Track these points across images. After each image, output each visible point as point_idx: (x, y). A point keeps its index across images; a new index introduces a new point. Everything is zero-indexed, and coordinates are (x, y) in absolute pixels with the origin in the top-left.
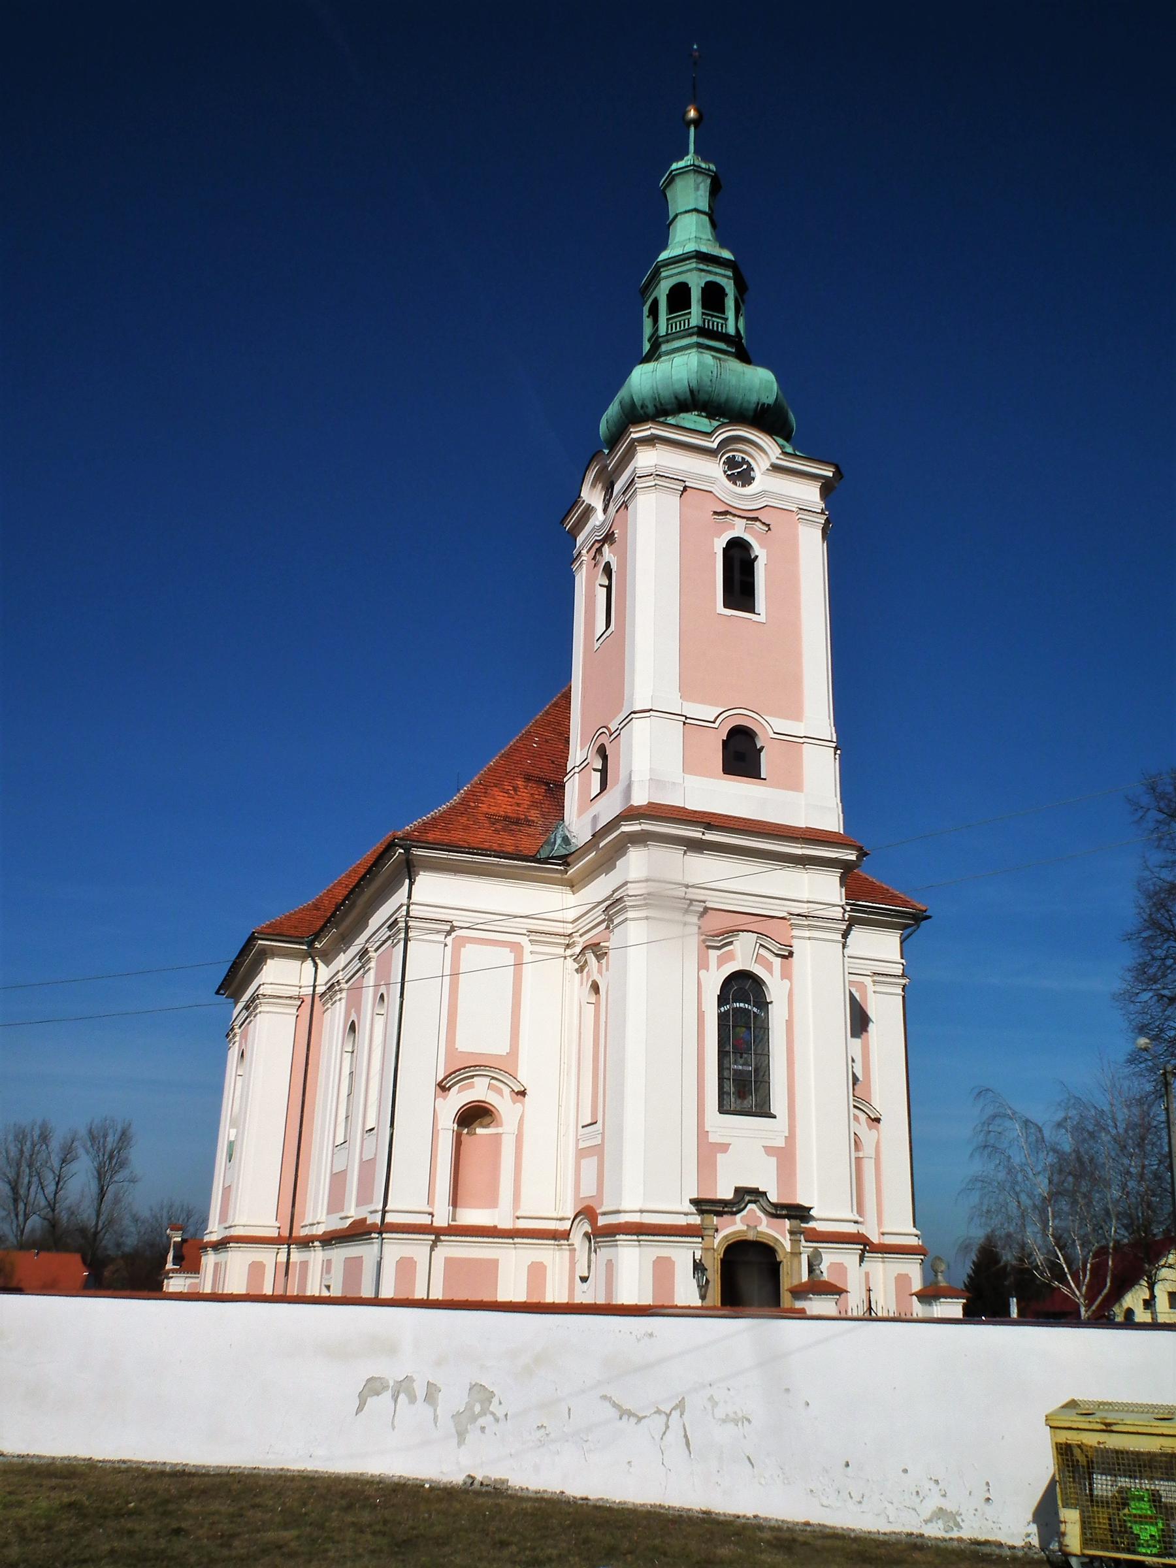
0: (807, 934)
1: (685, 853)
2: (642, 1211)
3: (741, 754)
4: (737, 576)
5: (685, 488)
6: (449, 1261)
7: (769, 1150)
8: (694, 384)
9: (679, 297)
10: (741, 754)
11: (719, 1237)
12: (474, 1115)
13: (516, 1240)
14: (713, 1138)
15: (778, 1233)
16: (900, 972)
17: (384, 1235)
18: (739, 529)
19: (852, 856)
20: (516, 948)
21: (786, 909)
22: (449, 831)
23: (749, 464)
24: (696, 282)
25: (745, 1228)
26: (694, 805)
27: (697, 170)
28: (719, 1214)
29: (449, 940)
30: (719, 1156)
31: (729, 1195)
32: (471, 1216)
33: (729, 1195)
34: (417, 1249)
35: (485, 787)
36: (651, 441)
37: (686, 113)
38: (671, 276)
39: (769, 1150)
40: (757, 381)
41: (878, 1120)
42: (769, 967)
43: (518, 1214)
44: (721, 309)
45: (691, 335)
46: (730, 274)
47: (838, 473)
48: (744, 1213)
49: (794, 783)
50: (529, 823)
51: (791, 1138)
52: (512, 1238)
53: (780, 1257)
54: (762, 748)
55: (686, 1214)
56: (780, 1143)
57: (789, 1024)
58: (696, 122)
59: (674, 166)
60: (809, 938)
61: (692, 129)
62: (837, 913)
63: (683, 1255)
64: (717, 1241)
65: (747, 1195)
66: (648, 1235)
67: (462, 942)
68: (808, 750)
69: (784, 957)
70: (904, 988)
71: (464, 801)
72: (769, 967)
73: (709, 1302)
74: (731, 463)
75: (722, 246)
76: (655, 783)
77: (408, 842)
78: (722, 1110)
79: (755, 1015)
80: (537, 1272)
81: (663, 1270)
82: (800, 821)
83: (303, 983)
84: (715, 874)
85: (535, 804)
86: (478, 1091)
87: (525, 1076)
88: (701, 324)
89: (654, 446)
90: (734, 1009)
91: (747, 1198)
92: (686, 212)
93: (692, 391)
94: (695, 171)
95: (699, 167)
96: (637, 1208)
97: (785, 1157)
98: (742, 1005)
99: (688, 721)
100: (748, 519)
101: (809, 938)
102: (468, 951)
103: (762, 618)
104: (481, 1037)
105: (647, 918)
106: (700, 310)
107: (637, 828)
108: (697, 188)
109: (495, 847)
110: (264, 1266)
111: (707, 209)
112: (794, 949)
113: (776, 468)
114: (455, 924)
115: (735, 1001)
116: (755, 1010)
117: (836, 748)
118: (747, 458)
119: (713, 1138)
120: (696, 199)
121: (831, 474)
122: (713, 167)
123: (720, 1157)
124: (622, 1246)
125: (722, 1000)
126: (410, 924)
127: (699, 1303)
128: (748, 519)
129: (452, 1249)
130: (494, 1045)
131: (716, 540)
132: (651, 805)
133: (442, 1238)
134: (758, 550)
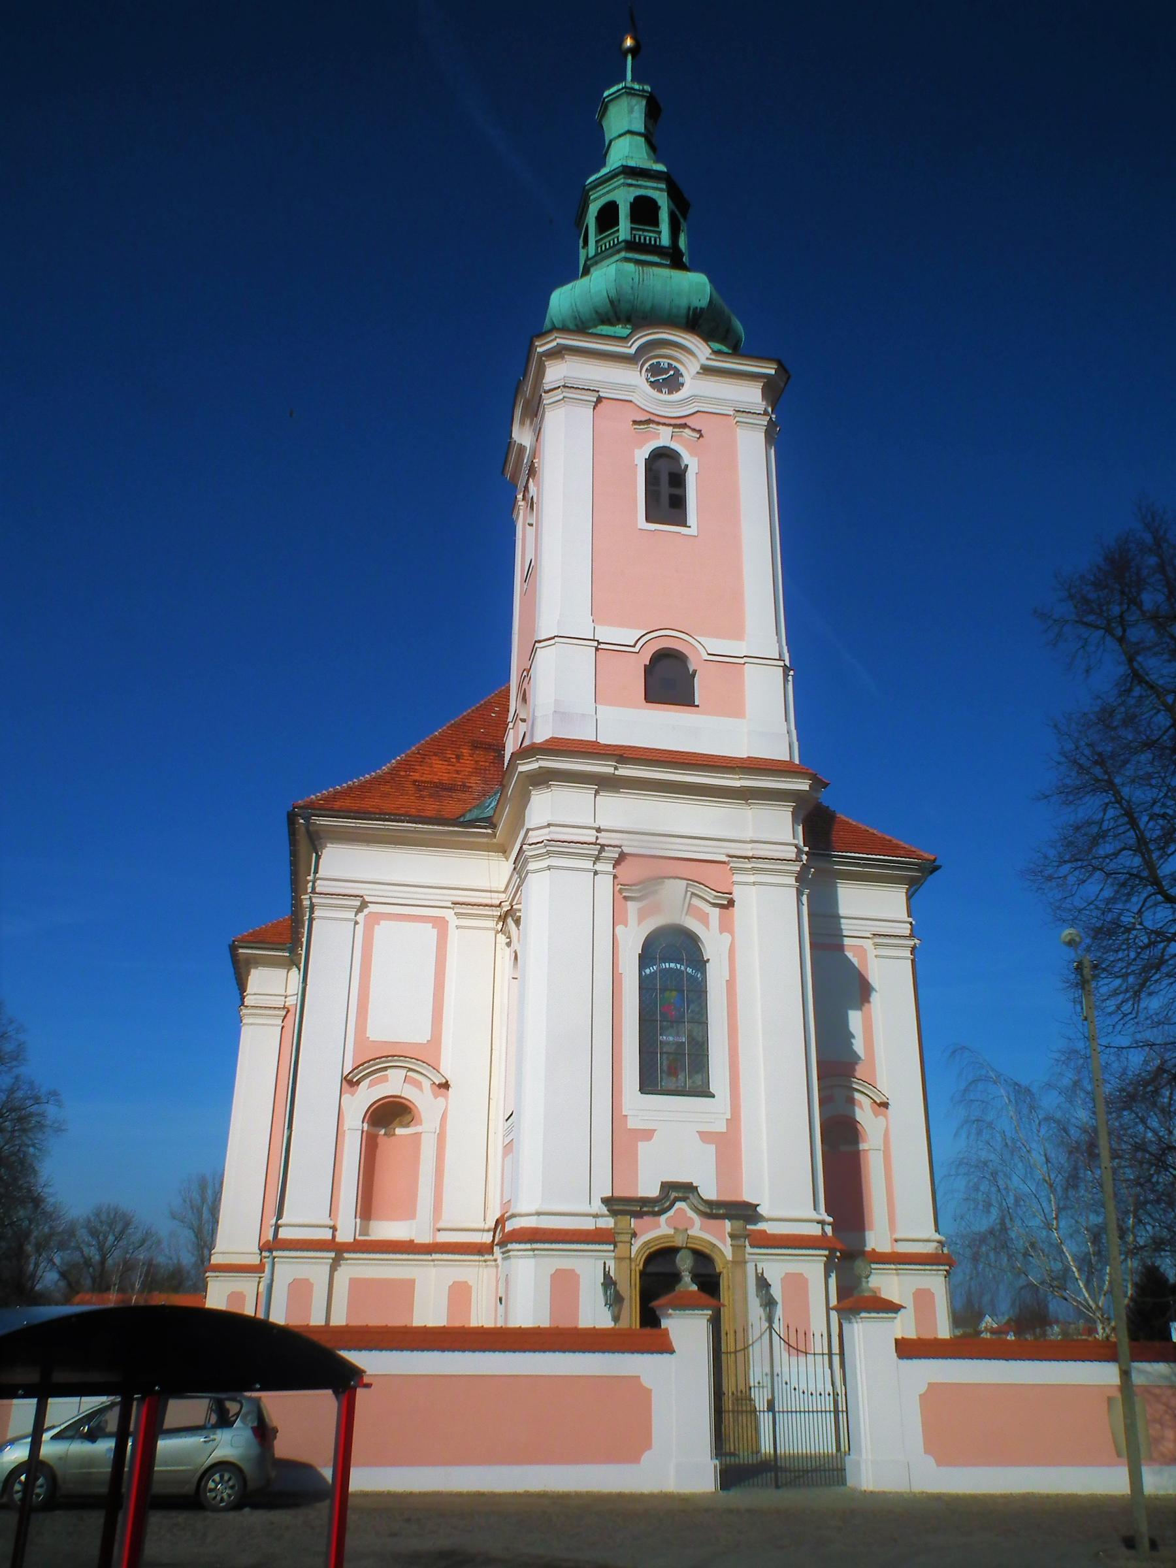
0: (752, 878)
1: (597, 793)
2: (538, 1214)
3: (668, 678)
4: (665, 490)
5: (600, 400)
6: (354, 1283)
7: (705, 1136)
8: (613, 293)
9: (608, 217)
10: (668, 678)
11: (637, 1244)
12: (389, 1114)
13: (435, 1256)
14: (632, 1124)
15: (717, 1238)
16: (908, 932)
17: (275, 1254)
18: (663, 438)
19: (803, 785)
20: (440, 924)
21: (723, 851)
22: (363, 799)
23: (676, 370)
24: (624, 196)
25: (672, 1232)
26: (608, 737)
27: (630, 92)
28: (639, 1215)
29: (361, 917)
30: (640, 1144)
31: (653, 1192)
32: (386, 1230)
33: (653, 1192)
34: (315, 1269)
35: (422, 757)
36: (558, 353)
37: (622, 41)
38: (600, 197)
39: (705, 1136)
40: (692, 286)
41: (885, 1105)
42: (704, 919)
43: (439, 1226)
44: (655, 222)
45: (618, 252)
46: (663, 186)
47: (782, 367)
48: (671, 1213)
49: (734, 708)
50: (465, 788)
51: (734, 1121)
52: (430, 1253)
53: (719, 1267)
54: (695, 672)
55: (596, 1216)
56: (722, 1128)
57: (731, 985)
58: (634, 51)
59: (606, 94)
60: (754, 884)
61: (629, 58)
62: (791, 853)
63: (589, 1268)
64: (634, 1249)
65: (677, 1191)
66: (544, 1242)
67: (377, 918)
68: (751, 672)
69: (722, 906)
70: (913, 949)
71: (394, 771)
72: (704, 919)
73: (624, 1324)
74: (655, 370)
75: (657, 161)
76: (560, 715)
77: (310, 806)
78: (644, 1089)
79: (690, 976)
80: (460, 1294)
81: (563, 1286)
82: (741, 750)
83: (289, 992)
84: (622, 813)
85: (477, 771)
86: (393, 1084)
87: (448, 1069)
88: (629, 238)
89: (563, 358)
90: (662, 971)
91: (673, 1195)
92: (620, 136)
93: (611, 302)
94: (628, 94)
95: (632, 89)
96: (533, 1211)
97: (727, 1145)
98: (672, 965)
99: (602, 646)
100: (675, 426)
101: (754, 884)
102: (383, 930)
103: (693, 531)
104: (397, 1020)
105: (549, 868)
106: (629, 225)
107: (535, 766)
108: (631, 111)
109: (413, 812)
110: (245, 1297)
111: (643, 130)
112: (735, 896)
113: (707, 370)
114: (367, 899)
115: (664, 960)
116: (689, 970)
117: (786, 669)
118: (674, 364)
119: (632, 1124)
120: (630, 122)
121: (773, 372)
122: (647, 88)
123: (642, 1146)
124: (516, 1256)
125: (645, 958)
126: (314, 900)
127: (611, 1324)
128: (675, 426)
129: (356, 1269)
130: (415, 1032)
131: (637, 451)
132: (553, 740)
133: (346, 1255)
134: (688, 459)
